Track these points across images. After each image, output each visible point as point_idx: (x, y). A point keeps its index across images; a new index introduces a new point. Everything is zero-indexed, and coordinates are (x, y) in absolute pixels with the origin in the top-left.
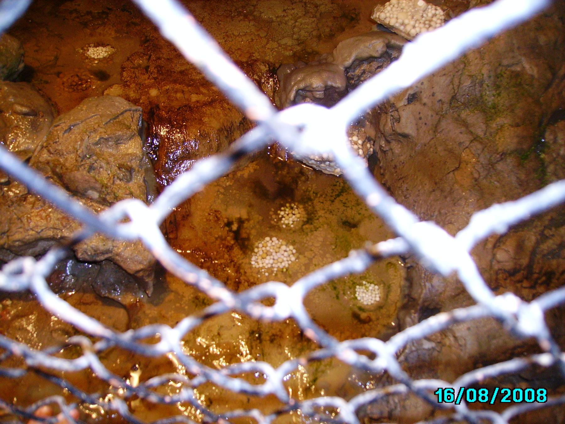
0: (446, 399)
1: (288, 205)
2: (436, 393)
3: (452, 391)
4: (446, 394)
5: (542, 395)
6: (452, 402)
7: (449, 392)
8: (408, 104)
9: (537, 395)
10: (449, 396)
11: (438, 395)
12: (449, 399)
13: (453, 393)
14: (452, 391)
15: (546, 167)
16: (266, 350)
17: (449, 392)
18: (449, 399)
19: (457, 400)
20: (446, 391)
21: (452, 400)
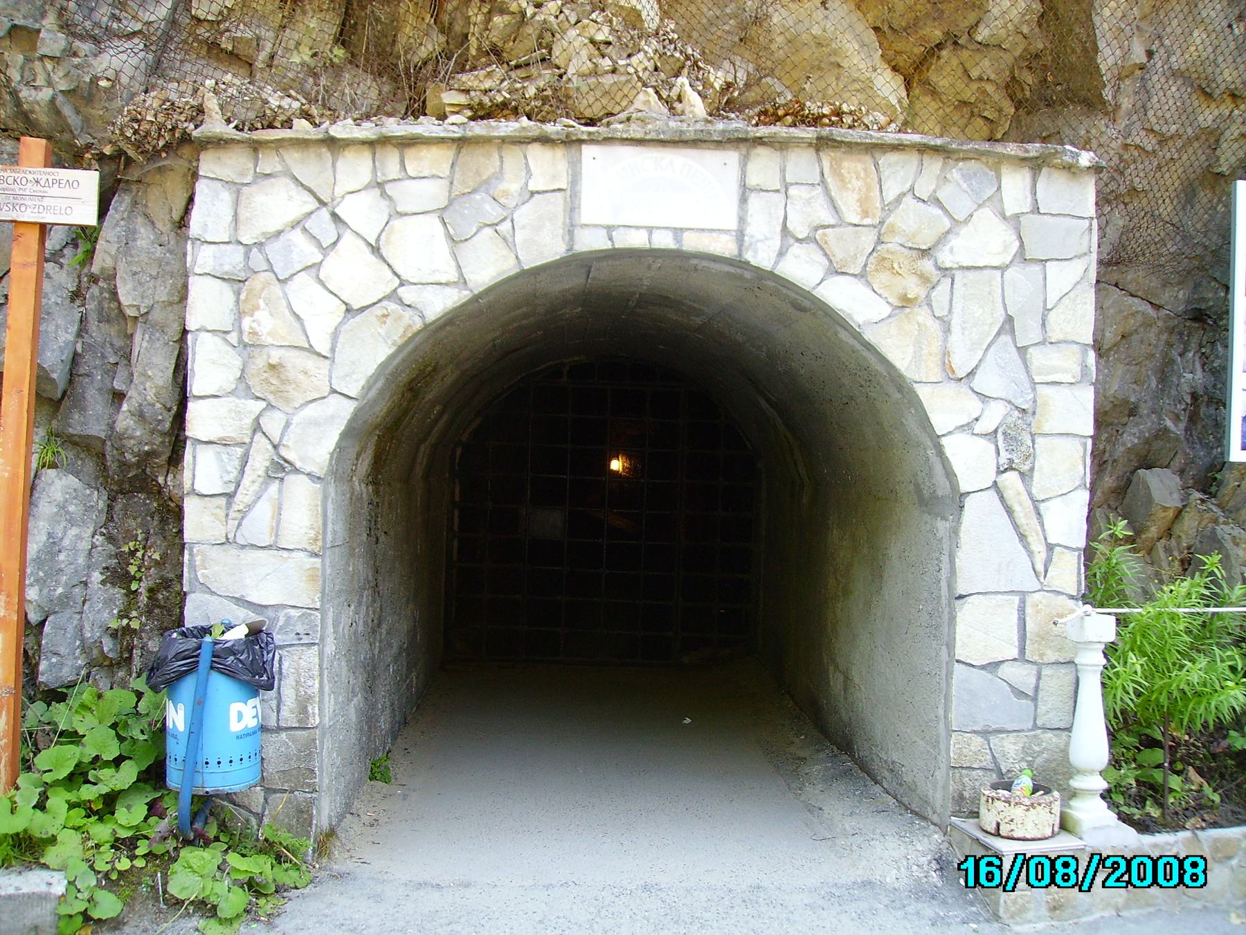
0: (983, 880)
1: (1179, 83)
2: (963, 867)
3: (997, 862)
4: (984, 870)
5: (1066, 871)
6: (997, 886)
7: (990, 864)
8: (1018, 348)
9: (1185, 872)
10: (991, 873)
11: (966, 870)
12: (1066, 881)
13: (1000, 867)
14: (997, 862)
15: (37, 664)
16: (337, 550)
17: (990, 864)
18: (1065, 881)
19: (1007, 881)
20: (983, 863)
21: (997, 881)
